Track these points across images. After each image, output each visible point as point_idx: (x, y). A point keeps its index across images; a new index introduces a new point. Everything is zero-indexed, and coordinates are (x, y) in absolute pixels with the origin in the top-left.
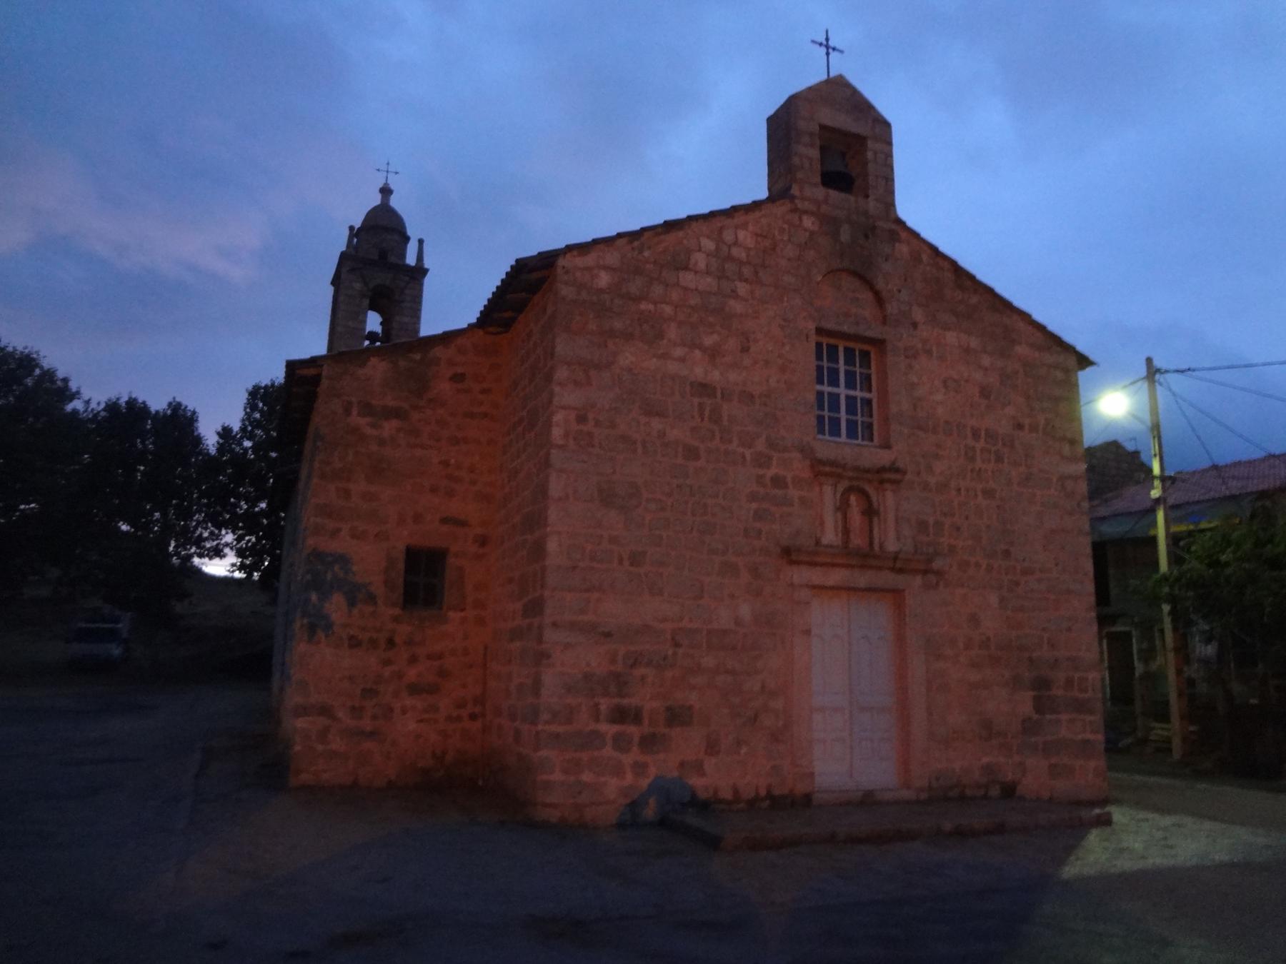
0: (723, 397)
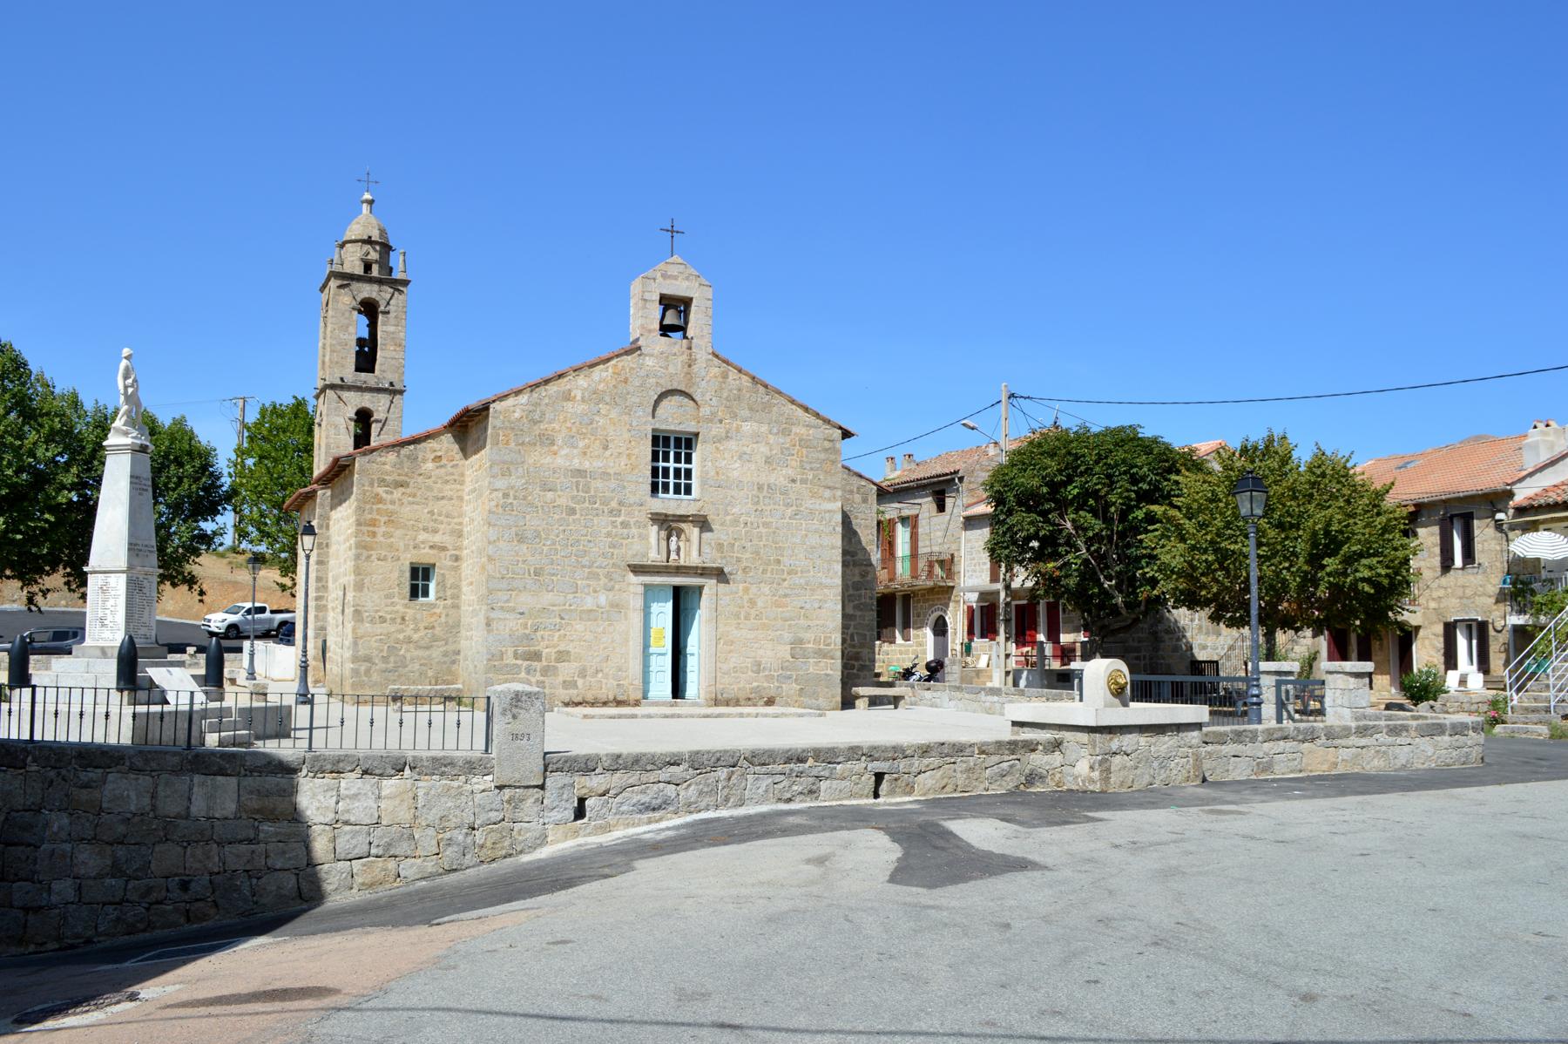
0: (586, 492)
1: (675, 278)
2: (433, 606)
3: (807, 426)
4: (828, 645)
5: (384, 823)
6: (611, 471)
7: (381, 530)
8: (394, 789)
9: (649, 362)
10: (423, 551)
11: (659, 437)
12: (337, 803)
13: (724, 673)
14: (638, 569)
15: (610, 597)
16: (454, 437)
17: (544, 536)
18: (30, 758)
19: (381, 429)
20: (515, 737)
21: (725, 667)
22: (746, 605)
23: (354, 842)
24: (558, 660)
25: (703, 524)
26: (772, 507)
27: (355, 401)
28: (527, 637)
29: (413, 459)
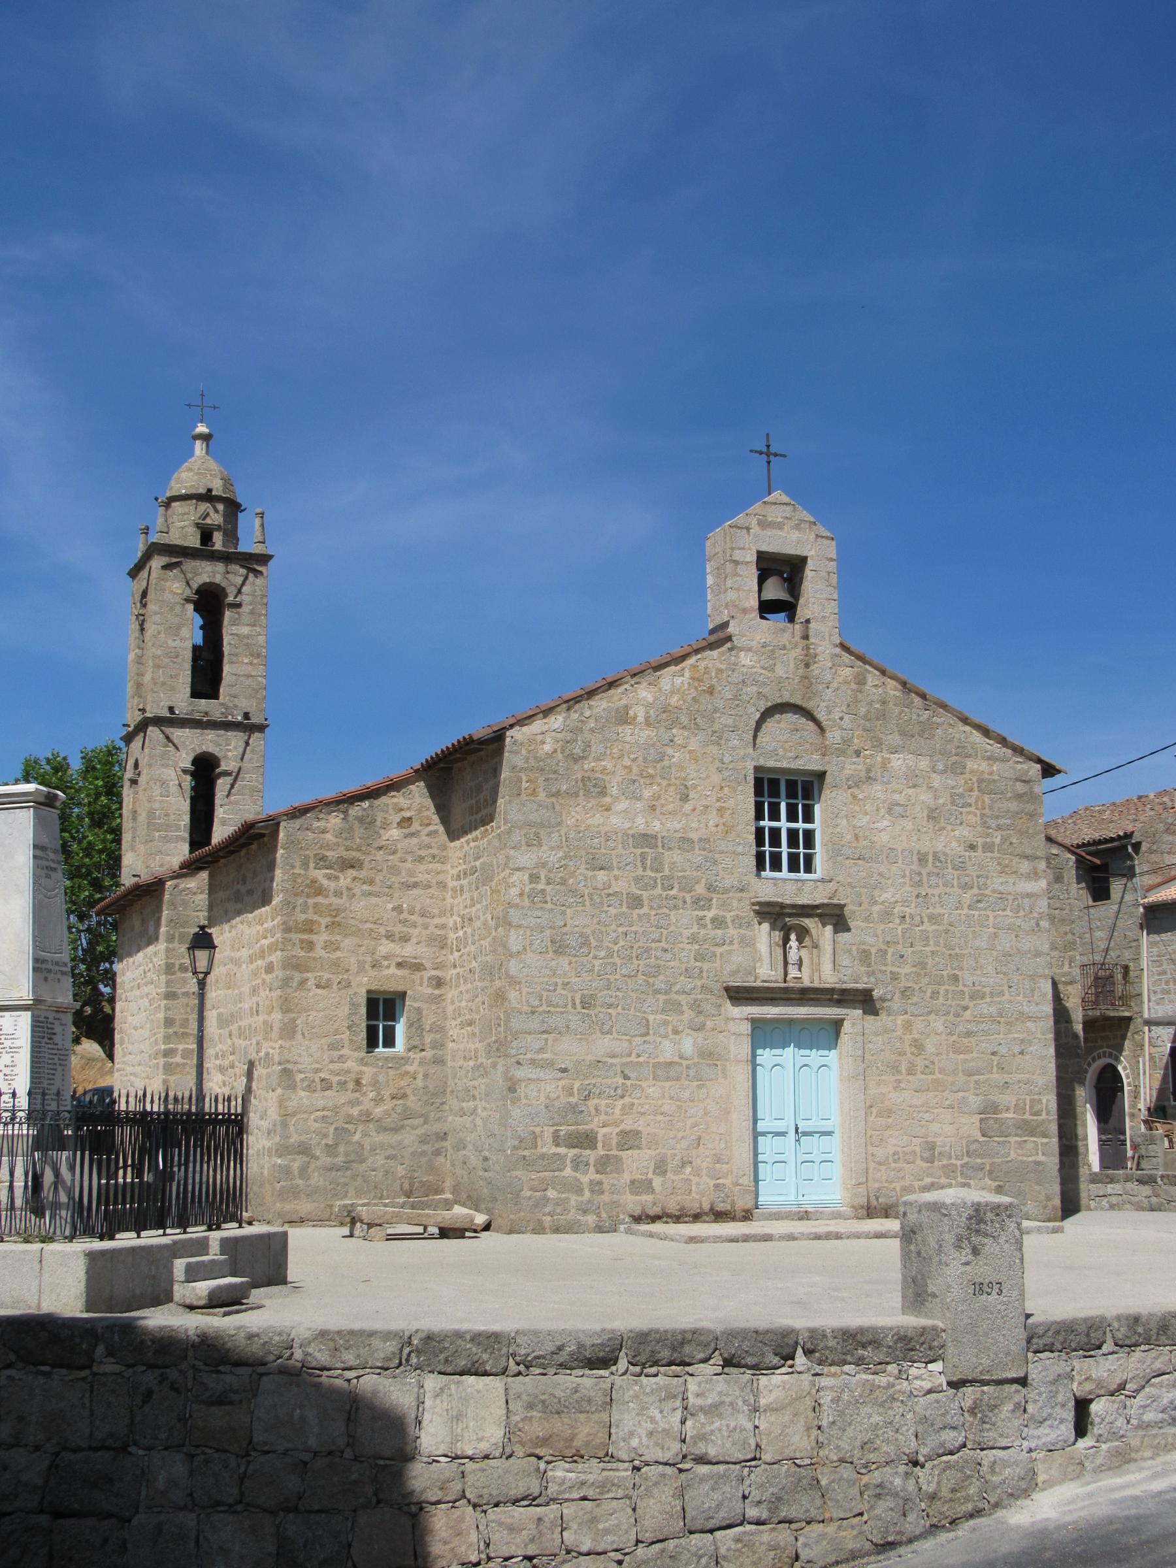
0: (657, 871)
1: (780, 526)
2: (405, 1060)
3: (989, 758)
4: (1038, 1113)
5: (767, 1457)
6: (694, 836)
7: (321, 938)
8: (777, 1394)
9: (745, 659)
10: (387, 972)
11: (796, 782)
12: (683, 1422)
13: (880, 1164)
14: (739, 995)
15: (700, 1040)
16: (429, 787)
17: (594, 943)
18: (100, 1350)
19: (232, 786)
20: (980, 1288)
21: (880, 1153)
22: (908, 1050)
23: (716, 1496)
24: (622, 1147)
25: (836, 917)
26: (941, 889)
27: (192, 742)
28: (573, 1108)
29: (367, 822)
